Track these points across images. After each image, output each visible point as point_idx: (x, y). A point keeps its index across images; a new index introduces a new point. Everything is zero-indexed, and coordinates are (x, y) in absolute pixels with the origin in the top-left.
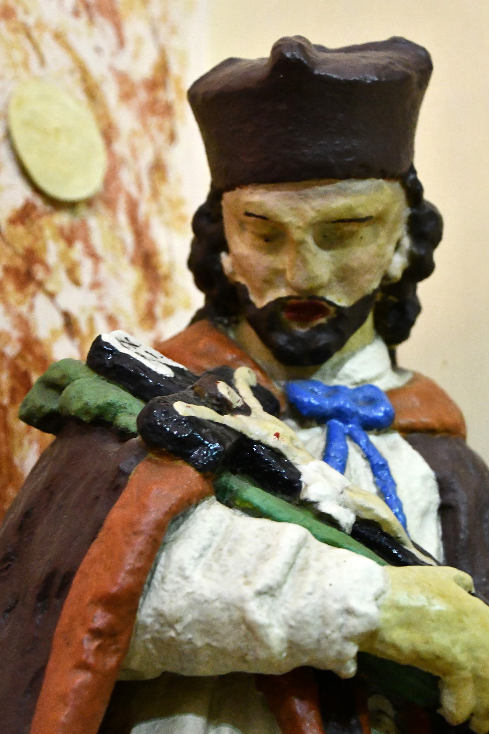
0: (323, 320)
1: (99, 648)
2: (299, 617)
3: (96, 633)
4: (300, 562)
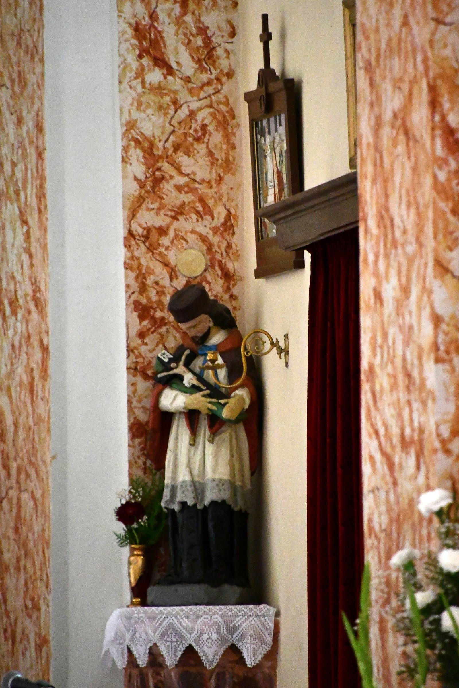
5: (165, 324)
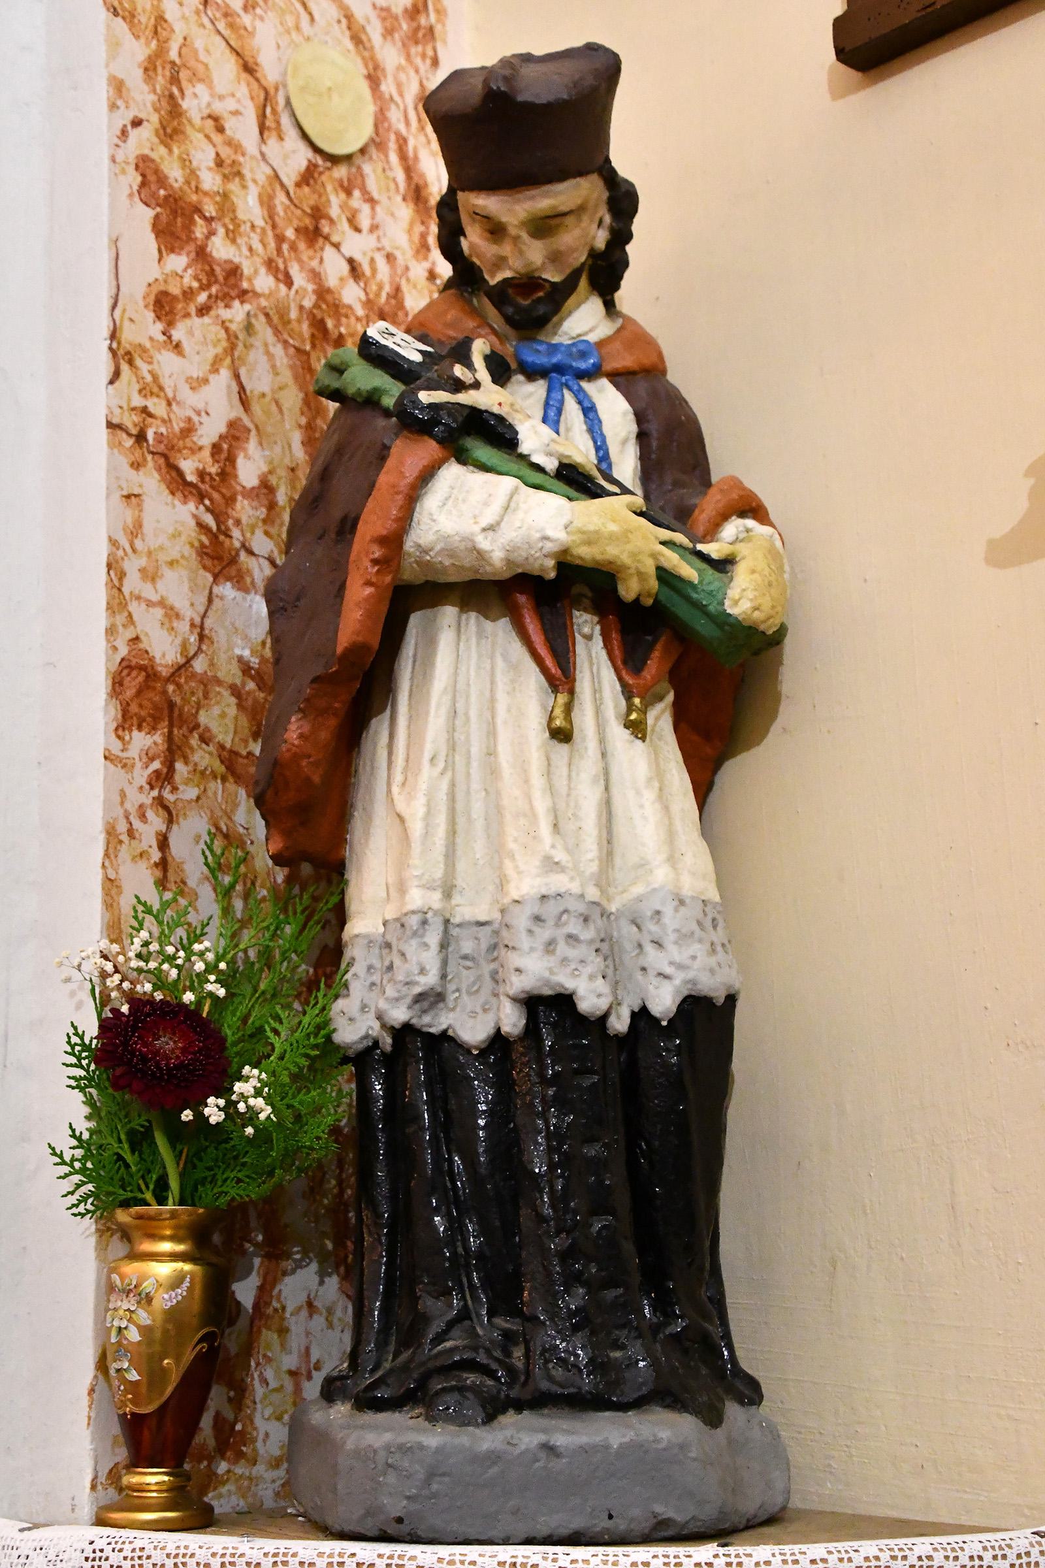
0: (541, 294)
1: (378, 571)
2: (512, 544)
3: (375, 562)
4: (513, 505)
5: (243, 295)
